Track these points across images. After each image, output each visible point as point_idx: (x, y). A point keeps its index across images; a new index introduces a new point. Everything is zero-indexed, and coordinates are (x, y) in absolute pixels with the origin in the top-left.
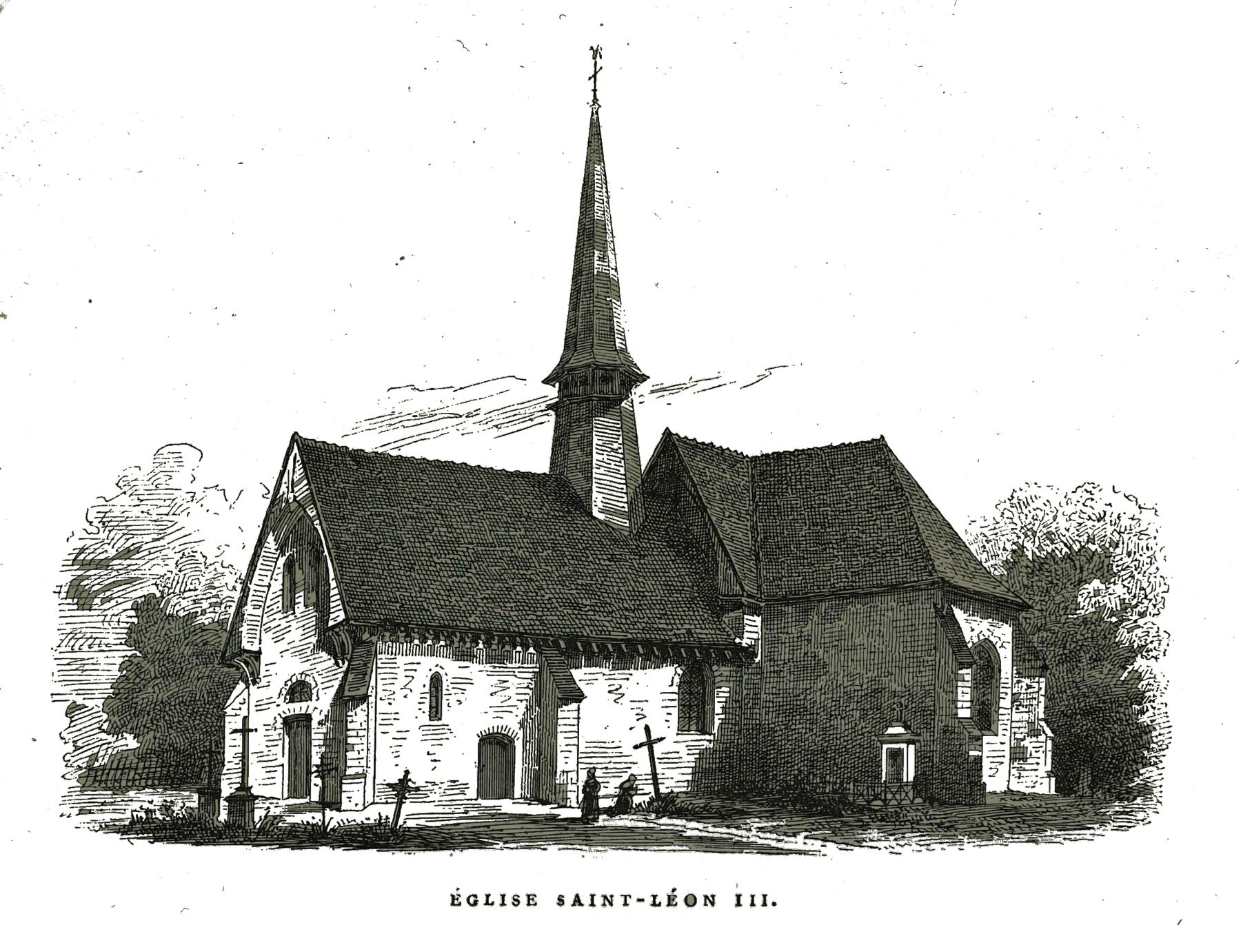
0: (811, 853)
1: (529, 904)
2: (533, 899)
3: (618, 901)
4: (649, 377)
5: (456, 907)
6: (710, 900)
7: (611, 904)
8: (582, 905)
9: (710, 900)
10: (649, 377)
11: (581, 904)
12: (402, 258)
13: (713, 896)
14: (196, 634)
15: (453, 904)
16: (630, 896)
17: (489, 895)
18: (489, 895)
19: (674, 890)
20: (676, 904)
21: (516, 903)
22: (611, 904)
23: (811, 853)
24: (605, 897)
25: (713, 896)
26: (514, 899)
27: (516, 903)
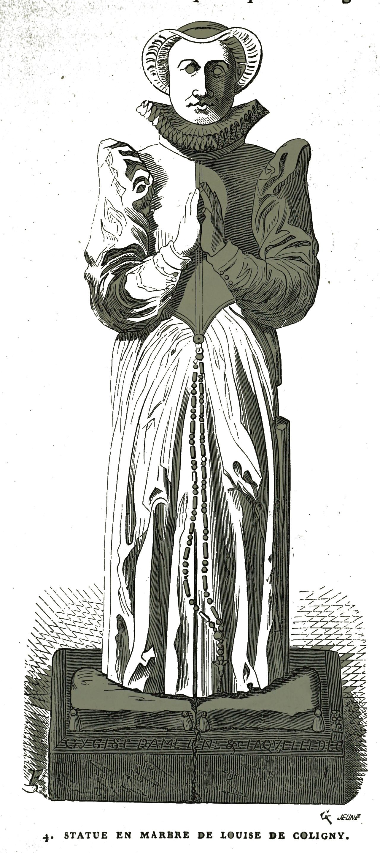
0: (120, 596)
1: (103, 838)
2: (105, 835)
3: (337, 836)
4: (25, 676)
5: (282, 839)
6: (128, 835)
7: (130, 837)
8: (84, 838)
9: (104, 835)
10: (25, 676)
11: (82, 838)
12: (364, 628)
13: (130, 833)
14: (92, 781)
15: (118, 837)
16: (75, 833)
17: (312, 833)
18: (312, 833)
19: (338, 819)
20: (260, 837)
21: (251, 837)
22: (130, 837)
23: (120, 596)
24: (126, 833)
25: (130, 833)
26: (66, 835)
27: (67, 837)
